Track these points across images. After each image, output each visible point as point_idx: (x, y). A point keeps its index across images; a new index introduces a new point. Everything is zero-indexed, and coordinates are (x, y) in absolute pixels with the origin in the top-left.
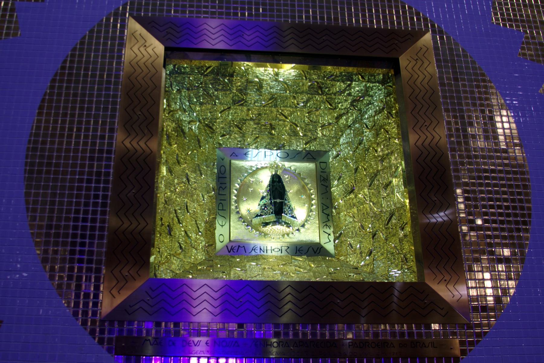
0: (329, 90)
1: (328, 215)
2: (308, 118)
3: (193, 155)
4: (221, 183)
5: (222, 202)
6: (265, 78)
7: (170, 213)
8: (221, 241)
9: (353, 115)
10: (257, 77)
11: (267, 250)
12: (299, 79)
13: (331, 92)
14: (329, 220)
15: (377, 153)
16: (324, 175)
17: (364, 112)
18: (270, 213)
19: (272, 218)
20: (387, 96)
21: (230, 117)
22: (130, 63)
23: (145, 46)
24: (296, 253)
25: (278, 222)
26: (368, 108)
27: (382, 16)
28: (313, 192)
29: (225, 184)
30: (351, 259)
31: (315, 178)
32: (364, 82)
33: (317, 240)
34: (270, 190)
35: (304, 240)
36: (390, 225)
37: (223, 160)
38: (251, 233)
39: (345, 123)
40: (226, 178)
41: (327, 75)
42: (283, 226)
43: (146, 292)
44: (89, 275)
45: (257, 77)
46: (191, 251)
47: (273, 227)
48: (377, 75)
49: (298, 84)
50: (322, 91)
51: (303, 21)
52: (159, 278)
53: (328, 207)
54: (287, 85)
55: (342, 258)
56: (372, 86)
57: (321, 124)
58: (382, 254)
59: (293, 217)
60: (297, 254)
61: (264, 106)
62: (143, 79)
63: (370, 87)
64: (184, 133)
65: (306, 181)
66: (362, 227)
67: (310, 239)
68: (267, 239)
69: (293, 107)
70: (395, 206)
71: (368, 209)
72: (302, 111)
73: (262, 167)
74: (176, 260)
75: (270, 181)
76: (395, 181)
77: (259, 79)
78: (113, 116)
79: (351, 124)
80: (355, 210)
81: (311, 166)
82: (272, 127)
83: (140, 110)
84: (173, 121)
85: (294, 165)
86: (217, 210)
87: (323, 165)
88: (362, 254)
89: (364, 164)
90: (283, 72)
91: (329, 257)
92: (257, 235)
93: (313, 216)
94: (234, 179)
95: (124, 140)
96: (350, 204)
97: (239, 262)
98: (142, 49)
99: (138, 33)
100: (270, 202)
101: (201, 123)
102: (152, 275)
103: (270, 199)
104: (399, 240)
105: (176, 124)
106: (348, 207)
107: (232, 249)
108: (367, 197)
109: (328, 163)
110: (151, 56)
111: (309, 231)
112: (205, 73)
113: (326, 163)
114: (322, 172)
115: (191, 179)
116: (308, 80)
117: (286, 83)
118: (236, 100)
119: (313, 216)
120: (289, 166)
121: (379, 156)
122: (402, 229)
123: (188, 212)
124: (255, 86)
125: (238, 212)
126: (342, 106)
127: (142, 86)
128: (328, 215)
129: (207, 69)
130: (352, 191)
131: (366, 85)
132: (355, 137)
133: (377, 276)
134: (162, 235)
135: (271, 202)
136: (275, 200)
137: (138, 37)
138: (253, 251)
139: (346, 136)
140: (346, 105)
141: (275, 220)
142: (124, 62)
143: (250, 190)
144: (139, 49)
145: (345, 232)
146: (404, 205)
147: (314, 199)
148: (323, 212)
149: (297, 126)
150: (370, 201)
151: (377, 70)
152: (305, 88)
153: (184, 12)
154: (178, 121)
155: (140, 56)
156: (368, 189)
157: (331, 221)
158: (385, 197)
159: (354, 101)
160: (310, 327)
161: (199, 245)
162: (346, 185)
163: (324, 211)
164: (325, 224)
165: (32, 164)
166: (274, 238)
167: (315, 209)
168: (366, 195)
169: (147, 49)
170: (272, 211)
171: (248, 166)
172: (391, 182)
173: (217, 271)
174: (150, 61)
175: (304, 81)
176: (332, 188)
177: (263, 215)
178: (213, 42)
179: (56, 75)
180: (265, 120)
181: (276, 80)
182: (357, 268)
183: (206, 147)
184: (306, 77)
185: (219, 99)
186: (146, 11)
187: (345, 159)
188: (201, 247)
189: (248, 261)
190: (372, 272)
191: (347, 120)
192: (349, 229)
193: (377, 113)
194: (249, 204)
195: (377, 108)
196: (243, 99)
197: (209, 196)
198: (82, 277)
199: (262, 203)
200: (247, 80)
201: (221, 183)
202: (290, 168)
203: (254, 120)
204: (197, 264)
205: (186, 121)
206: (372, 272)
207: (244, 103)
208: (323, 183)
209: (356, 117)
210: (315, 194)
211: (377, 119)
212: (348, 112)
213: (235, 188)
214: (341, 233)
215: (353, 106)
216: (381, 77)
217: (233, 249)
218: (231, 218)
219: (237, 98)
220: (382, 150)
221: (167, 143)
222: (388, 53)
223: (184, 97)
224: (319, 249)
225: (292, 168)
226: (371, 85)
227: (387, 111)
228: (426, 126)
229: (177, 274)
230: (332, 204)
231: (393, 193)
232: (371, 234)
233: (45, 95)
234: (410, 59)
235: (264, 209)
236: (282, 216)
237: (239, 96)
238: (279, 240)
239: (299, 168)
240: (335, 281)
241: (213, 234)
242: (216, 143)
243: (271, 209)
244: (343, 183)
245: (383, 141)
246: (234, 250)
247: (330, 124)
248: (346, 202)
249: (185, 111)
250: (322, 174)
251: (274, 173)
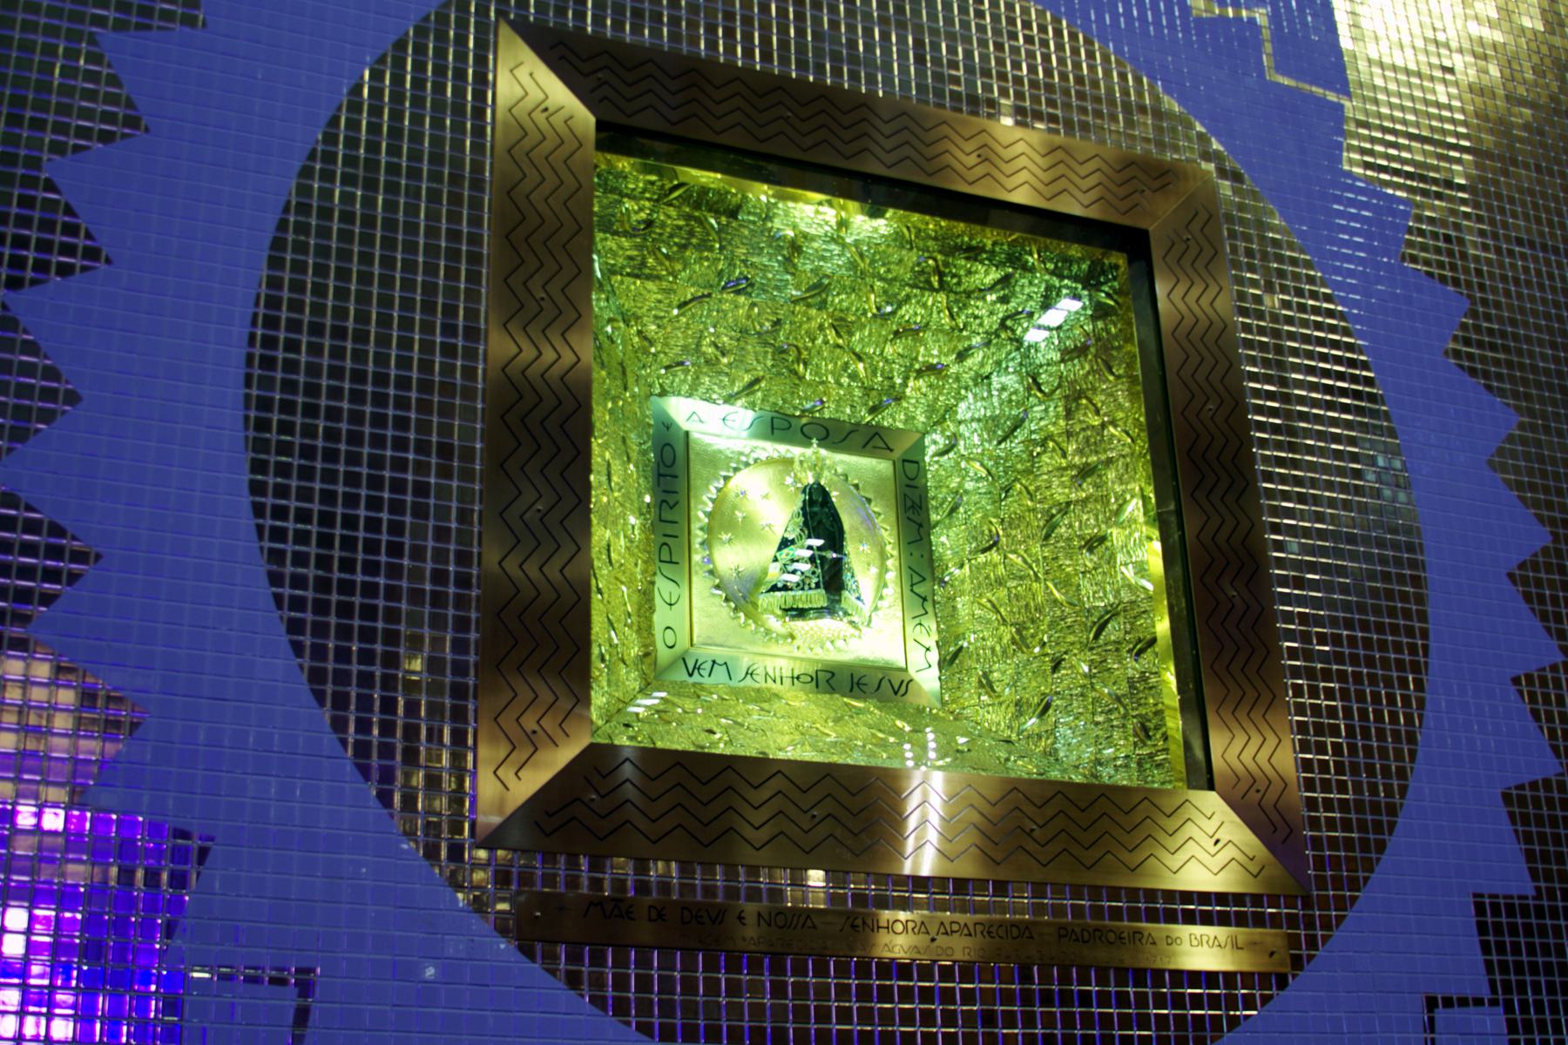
1: (925, 599)
18: (813, 585)
19: (819, 598)
27: (760, 36)
31: (893, 501)
35: (871, 658)
40: (676, 477)
43: (585, 778)
44: (436, 724)
50: (941, 282)
51: (547, 21)
53: (924, 579)
59: (858, 598)
70: (1115, 597)
78: (473, 296)
83: (543, 287)
85: (843, 462)
86: (657, 561)
94: (699, 482)
109: (922, 464)
114: (908, 486)
160: (562, 859)
163: (916, 589)
165: (265, 404)
170: (815, 580)
178: (889, 159)
179: (312, 156)
198: (417, 728)
208: (910, 514)
222: (762, 142)
233: (286, 210)
241: (650, 627)
250: (908, 492)
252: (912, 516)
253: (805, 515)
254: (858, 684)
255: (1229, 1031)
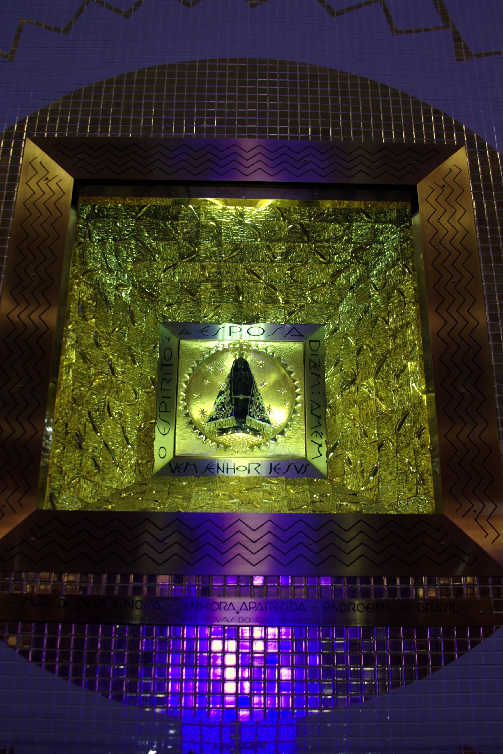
0: (319, 236)
1: (320, 417)
2: (291, 277)
3: (122, 333)
4: (164, 374)
5: (165, 400)
6: (224, 220)
7: (81, 416)
8: (162, 456)
9: (356, 271)
10: (213, 219)
11: (227, 469)
12: (273, 220)
13: (322, 238)
14: (320, 425)
15: (387, 326)
16: (316, 359)
17: (371, 266)
19: (230, 421)
20: (403, 242)
21: (178, 278)
22: (24, 204)
23: (47, 179)
24: (270, 473)
25: (240, 427)
26: (378, 260)
28: (299, 384)
29: (171, 374)
30: (348, 481)
32: (369, 222)
33: (302, 454)
34: (230, 382)
35: (283, 453)
36: (402, 431)
37: (169, 340)
38: (205, 445)
39: (345, 282)
40: (172, 365)
41: (314, 214)
42: (249, 433)
45: (213, 219)
46: (113, 471)
47: (233, 435)
48: (388, 212)
49: (273, 228)
50: (308, 238)
52: (60, 509)
53: (320, 406)
54: (257, 230)
55: (337, 480)
56: (383, 228)
57: (310, 285)
58: (391, 474)
59: (263, 420)
60: (271, 474)
61: (225, 261)
62: (41, 225)
63: (379, 229)
64: (107, 302)
65: (288, 368)
66: (365, 434)
67: (292, 453)
68: (227, 453)
69: (266, 262)
71: (374, 408)
72: (281, 266)
73: (225, 349)
74: (87, 484)
75: (232, 369)
76: (411, 366)
77: (215, 222)
79: (354, 285)
80: (355, 409)
81: (297, 346)
82: (239, 291)
84: (91, 285)
85: (271, 346)
87: (314, 345)
88: (363, 473)
89: (370, 342)
90: (249, 211)
91: (318, 478)
92: (214, 447)
93: (297, 419)
95: (458, 349)
96: (350, 401)
97: (184, 487)
98: (42, 184)
99: (38, 160)
100: (229, 399)
101: (136, 288)
102: (46, 506)
103: (230, 395)
104: (415, 453)
105: (94, 289)
106: (346, 404)
107: (177, 467)
108: (373, 390)
110: (54, 193)
111: (291, 441)
112: (139, 215)
113: (319, 341)
114: (312, 355)
115: (117, 368)
116: (287, 221)
117: (255, 228)
118: (184, 253)
119: (297, 419)
120: (265, 347)
121: (390, 329)
122: (419, 435)
123: (110, 415)
124: (210, 232)
125: (187, 415)
126: (339, 258)
127: (39, 236)
128: (320, 417)
129: (140, 210)
130: (353, 382)
131: (373, 227)
132: (359, 302)
133: (383, 505)
134: (66, 447)
135: (231, 398)
136: (237, 397)
137: (38, 167)
138: (208, 470)
139: (347, 302)
140: (346, 256)
141: (235, 425)
142: (15, 202)
143: (206, 382)
144: (37, 184)
145: (342, 442)
146: (421, 402)
147: (300, 395)
148: (312, 413)
149: (276, 290)
150: (377, 395)
151: (391, 203)
152: (284, 233)
153: (105, 129)
154: (98, 284)
155: (39, 192)
156: (374, 378)
157: (323, 426)
158: (397, 390)
159: (355, 251)
161: (126, 463)
162: (345, 372)
163: (314, 412)
164: (314, 430)
166: (238, 452)
167: (300, 408)
168: (371, 387)
169: (48, 184)
170: (230, 412)
171: (204, 348)
172: (405, 366)
173: (147, 500)
174: (53, 199)
175: (282, 223)
176: (327, 378)
177: (219, 419)
180: (227, 282)
181: (241, 223)
182: (355, 495)
183: (142, 324)
184: (284, 218)
185: (159, 253)
186: (52, 130)
187: (345, 336)
188: (129, 466)
189: (197, 485)
190: (377, 501)
191: (347, 278)
192: (347, 436)
193: (388, 267)
194: (204, 403)
195: (390, 259)
196: (194, 252)
197: (145, 392)
199: (218, 401)
200: (199, 223)
201: (164, 374)
202: (266, 349)
203: (211, 281)
204: (123, 490)
205: (111, 284)
206: (377, 501)
207: (196, 257)
208: (313, 370)
209: (360, 274)
210: (302, 388)
211: (390, 275)
212: (348, 267)
213: (184, 380)
214: (337, 443)
215: (356, 257)
216: (394, 214)
217: (178, 468)
218: (177, 423)
219: (185, 250)
220: (394, 320)
221: (79, 316)
223: (109, 251)
224: (304, 468)
225: (269, 350)
226: (381, 227)
227: (402, 264)
228: (454, 282)
229: (88, 504)
230: (325, 401)
231: (408, 383)
232: (376, 444)
234: (433, 185)
235: (221, 410)
236: (245, 419)
237: (187, 247)
238: (244, 454)
239: (279, 349)
240: (318, 512)
242: (159, 316)
243: (230, 408)
244: (341, 370)
245: (397, 307)
246: (180, 470)
247: (324, 285)
248: (344, 397)
249: (111, 271)
250: (312, 358)
251: (238, 357)
252: (314, 372)
253: (230, 377)
254: (274, 469)
255: (445, 665)
